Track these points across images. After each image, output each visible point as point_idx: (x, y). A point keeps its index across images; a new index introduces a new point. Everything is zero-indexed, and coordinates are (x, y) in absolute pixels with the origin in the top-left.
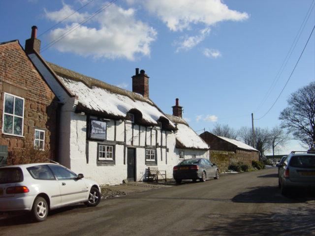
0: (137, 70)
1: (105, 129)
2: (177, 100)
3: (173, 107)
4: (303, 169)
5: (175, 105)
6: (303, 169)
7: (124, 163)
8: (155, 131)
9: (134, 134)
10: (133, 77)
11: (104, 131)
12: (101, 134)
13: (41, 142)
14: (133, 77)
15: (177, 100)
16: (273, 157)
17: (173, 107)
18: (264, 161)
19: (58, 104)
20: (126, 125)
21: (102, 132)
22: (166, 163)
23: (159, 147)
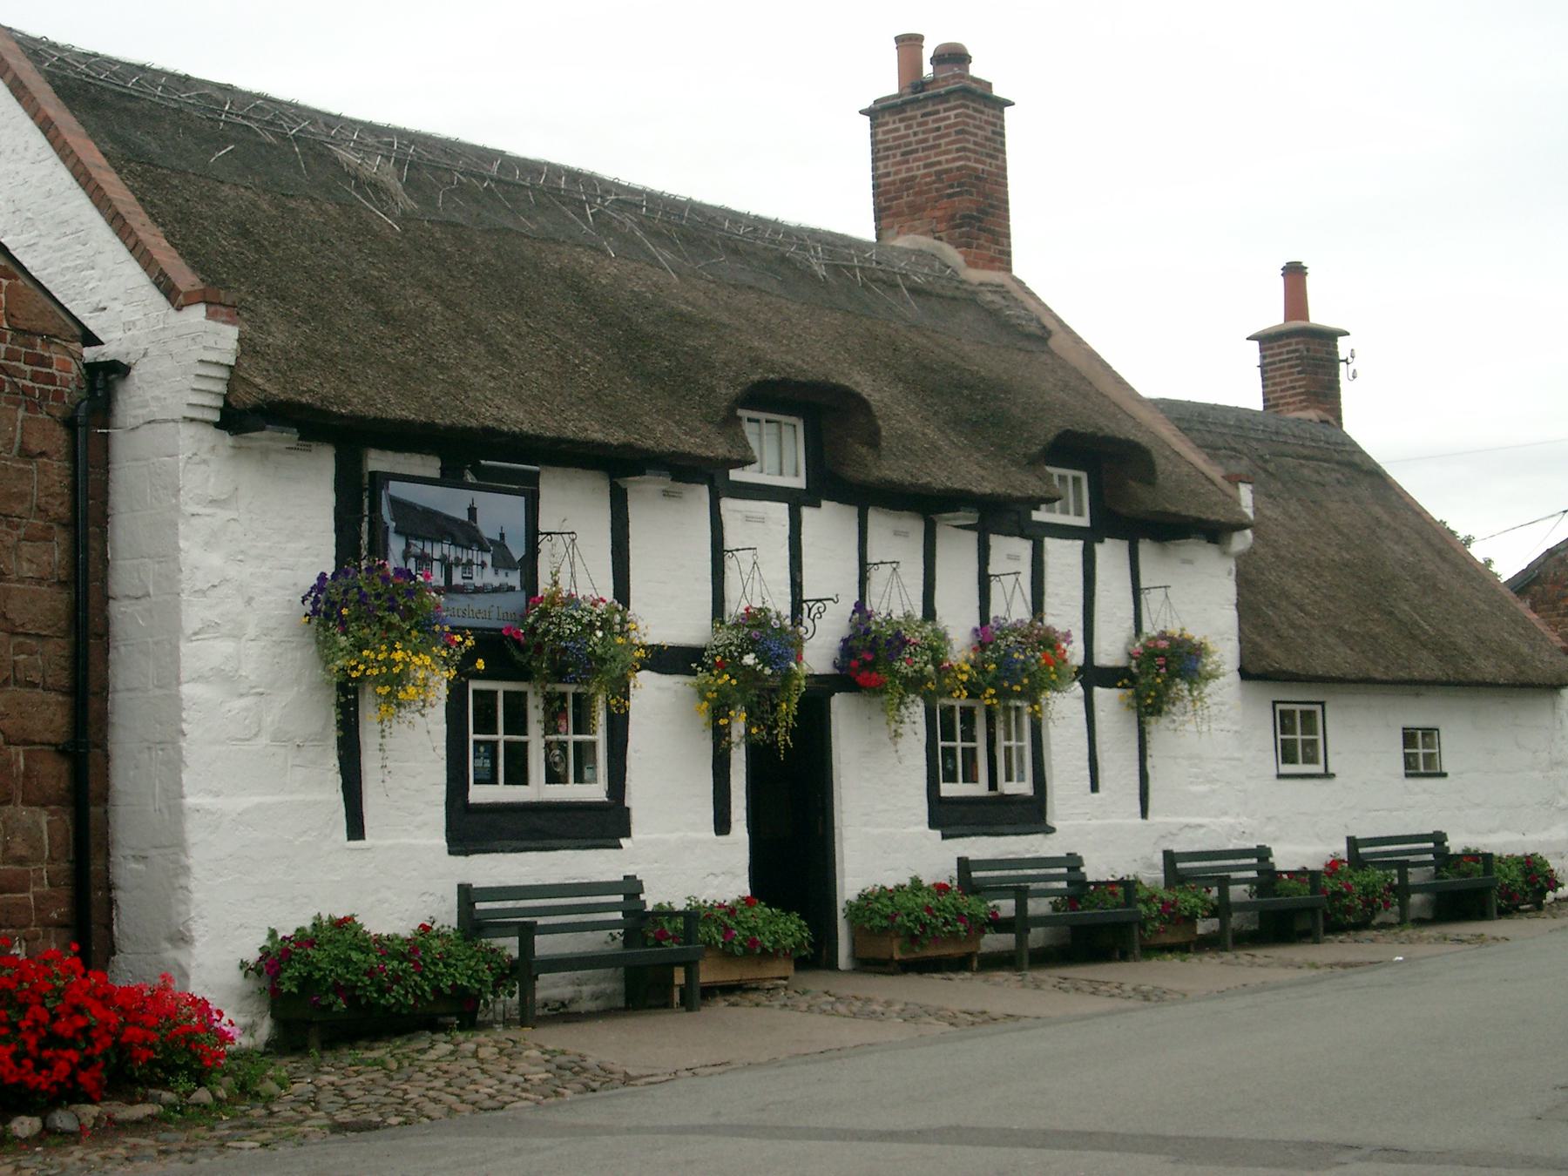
0: (909, 44)
1: (518, 552)
2: (1295, 274)
3: (1266, 340)
4: (1013, 724)
5: (1273, 316)
6: (1013, 724)
7: (722, 825)
8: (1023, 548)
9: (1001, 589)
10: (878, 113)
11: (503, 561)
12: (478, 590)
13: (1008, 738)
14: (878, 113)
15: (1295, 274)
16: (869, 268)
17: (1266, 340)
18: (1446, 610)
19: (93, 369)
20: (728, 506)
21: (488, 577)
22: (1144, 813)
23: (1109, 677)
